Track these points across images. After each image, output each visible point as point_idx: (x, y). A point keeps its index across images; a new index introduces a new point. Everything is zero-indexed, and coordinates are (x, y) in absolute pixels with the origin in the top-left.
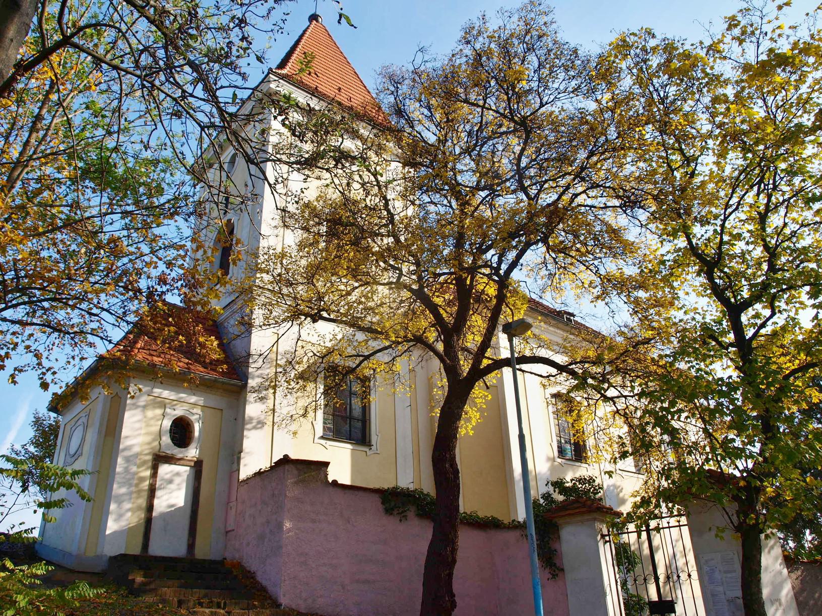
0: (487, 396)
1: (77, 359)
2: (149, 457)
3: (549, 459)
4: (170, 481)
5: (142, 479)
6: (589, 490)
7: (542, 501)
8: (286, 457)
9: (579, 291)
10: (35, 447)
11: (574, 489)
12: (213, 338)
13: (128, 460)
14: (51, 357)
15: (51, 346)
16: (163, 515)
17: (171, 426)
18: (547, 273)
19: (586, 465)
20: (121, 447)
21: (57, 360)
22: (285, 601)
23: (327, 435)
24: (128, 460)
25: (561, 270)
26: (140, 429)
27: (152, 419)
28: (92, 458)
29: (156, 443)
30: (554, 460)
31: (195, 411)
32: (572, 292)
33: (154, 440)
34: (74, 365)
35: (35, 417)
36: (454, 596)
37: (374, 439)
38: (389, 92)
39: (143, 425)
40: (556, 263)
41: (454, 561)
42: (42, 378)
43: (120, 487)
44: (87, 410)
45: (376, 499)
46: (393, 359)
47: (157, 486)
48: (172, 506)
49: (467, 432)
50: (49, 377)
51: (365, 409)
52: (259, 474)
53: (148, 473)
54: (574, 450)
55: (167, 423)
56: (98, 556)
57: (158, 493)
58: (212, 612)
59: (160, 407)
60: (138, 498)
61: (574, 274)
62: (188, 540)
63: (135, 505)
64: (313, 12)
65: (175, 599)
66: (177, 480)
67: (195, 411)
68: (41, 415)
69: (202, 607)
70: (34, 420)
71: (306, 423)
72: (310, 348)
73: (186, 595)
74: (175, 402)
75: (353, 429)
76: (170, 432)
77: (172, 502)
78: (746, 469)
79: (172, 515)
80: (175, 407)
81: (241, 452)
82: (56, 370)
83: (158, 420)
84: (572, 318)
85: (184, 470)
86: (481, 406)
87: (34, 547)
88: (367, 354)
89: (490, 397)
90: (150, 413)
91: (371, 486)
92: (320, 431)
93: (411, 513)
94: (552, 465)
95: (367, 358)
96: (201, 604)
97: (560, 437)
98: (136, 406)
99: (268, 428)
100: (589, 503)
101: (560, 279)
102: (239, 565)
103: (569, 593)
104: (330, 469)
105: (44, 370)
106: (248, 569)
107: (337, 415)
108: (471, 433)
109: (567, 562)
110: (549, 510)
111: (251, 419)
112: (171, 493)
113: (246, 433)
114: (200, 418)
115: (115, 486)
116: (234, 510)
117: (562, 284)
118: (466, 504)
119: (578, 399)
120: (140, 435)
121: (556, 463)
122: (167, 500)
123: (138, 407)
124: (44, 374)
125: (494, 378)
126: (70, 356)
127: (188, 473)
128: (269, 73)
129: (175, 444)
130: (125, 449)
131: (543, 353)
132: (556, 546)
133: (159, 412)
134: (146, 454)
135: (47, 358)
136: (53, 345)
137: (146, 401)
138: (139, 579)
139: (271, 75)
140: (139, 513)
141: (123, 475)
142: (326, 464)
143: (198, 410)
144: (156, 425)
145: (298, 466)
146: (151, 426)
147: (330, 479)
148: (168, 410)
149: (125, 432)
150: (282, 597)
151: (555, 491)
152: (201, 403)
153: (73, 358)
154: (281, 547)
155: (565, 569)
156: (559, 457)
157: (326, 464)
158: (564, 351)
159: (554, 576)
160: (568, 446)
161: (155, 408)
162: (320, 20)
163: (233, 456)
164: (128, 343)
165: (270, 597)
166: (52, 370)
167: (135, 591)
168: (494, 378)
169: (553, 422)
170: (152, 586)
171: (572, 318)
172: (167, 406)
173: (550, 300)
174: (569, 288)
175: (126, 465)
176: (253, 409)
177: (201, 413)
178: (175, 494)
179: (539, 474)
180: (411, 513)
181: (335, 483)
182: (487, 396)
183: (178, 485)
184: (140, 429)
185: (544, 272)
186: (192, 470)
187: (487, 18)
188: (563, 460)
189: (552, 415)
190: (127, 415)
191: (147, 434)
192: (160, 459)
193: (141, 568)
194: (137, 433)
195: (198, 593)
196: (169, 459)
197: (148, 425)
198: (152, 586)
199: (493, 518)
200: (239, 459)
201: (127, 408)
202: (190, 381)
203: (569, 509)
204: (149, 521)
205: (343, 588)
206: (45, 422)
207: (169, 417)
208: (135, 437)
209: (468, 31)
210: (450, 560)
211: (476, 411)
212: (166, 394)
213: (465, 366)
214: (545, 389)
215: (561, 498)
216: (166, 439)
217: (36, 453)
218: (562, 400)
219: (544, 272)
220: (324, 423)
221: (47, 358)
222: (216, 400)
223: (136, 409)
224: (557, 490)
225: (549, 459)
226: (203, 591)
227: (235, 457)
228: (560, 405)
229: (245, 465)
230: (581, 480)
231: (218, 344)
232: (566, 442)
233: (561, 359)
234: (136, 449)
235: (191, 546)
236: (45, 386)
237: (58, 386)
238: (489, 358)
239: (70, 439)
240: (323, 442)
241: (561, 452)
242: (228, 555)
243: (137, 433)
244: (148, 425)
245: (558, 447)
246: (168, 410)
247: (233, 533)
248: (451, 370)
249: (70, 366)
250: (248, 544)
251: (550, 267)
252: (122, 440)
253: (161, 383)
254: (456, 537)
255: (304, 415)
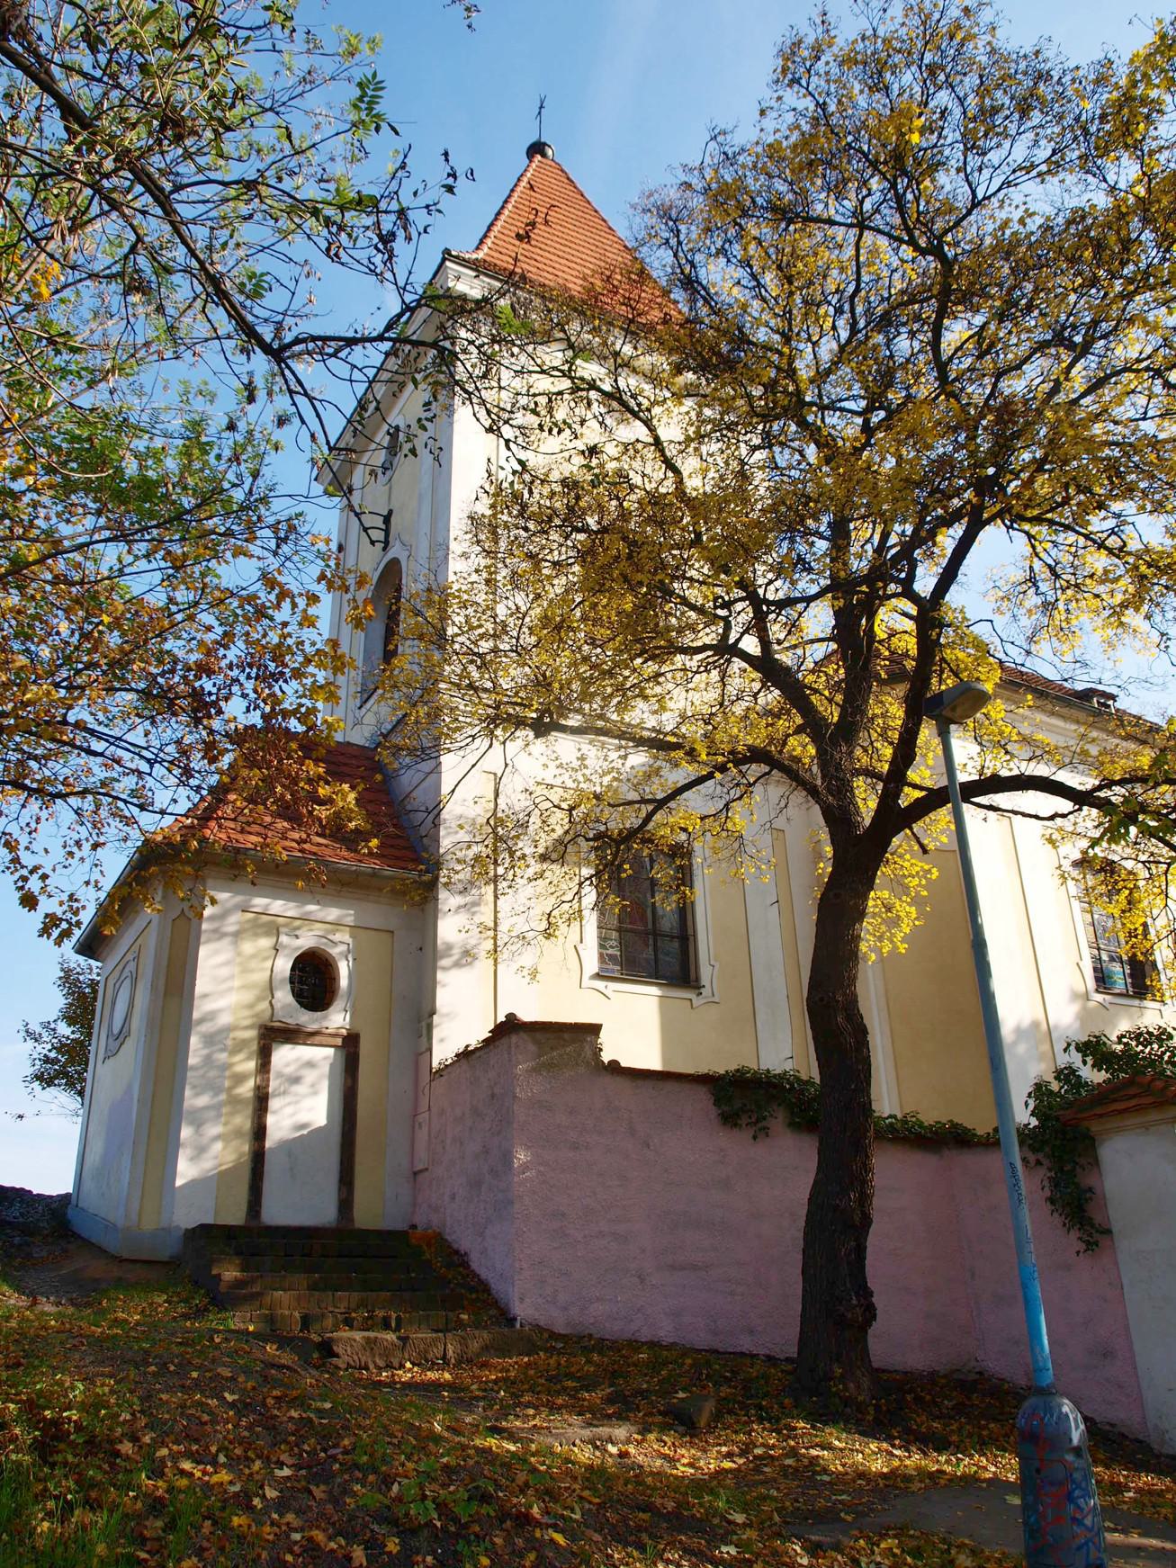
0: (929, 871)
1: (87, 846)
2: (252, 1033)
3: (1075, 996)
4: (296, 1080)
5: (240, 1079)
6: (1161, 1057)
7: (1055, 1086)
8: (511, 1017)
9: (1110, 632)
10: (69, 1025)
11: (1128, 1056)
12: (346, 787)
13: (210, 1040)
14: (34, 847)
15: (33, 825)
16: (288, 1146)
17: (293, 969)
18: (1039, 600)
19: (1157, 1005)
20: (196, 1015)
21: (46, 851)
22: (523, 1310)
23: (607, 970)
24: (210, 1040)
25: (1069, 592)
26: (232, 977)
27: (253, 956)
28: (142, 1043)
29: (264, 1005)
30: (1087, 997)
31: (337, 937)
32: (1097, 637)
33: (259, 999)
34: (82, 859)
35: (62, 970)
36: (871, 1294)
37: (706, 974)
38: (657, 241)
39: (237, 970)
40: (1057, 576)
41: (866, 1221)
42: (22, 888)
43: (197, 1095)
44: (135, 948)
45: (702, 1096)
46: (727, 806)
47: (270, 1090)
48: (303, 1126)
49: (895, 947)
50: (34, 884)
51: (685, 912)
52: (465, 1055)
53: (251, 1065)
54: (1131, 975)
55: (284, 965)
56: (163, 1229)
57: (274, 1104)
58: (368, 1339)
59: (267, 934)
60: (232, 1114)
61: (1097, 596)
62: (340, 1190)
63: (230, 1127)
64: (534, 139)
65: (297, 1314)
66: (310, 1076)
67: (337, 937)
68: (73, 965)
69: (352, 1328)
70: (62, 974)
71: (555, 951)
72: (545, 792)
73: (323, 1305)
74: (298, 923)
75: (661, 956)
76: (291, 982)
77: (303, 1117)
78: (936, 379)
79: (306, 1142)
80: (297, 933)
81: (433, 1012)
82: (48, 871)
83: (266, 959)
84: (1110, 702)
85: (323, 1055)
86: (918, 893)
87: (65, 1214)
88: (660, 796)
89: (935, 874)
90: (248, 947)
91: (691, 1071)
92: (592, 965)
93: (778, 1120)
94: (1084, 1008)
95: (660, 804)
96: (349, 1323)
97: (1099, 949)
98: (219, 934)
99: (484, 965)
100: (1159, 1084)
101: (1068, 611)
102: (438, 1241)
103: (1125, 1281)
104: (604, 1037)
105: (25, 872)
106: (455, 1246)
107: (627, 930)
108: (902, 948)
109: (1117, 1215)
110: (1070, 1104)
111: (449, 947)
112: (297, 1102)
113: (440, 976)
114: (349, 951)
115: (188, 1093)
116: (425, 1129)
117: (1074, 622)
118: (887, 1100)
119: (1129, 864)
120: (230, 989)
121: (1091, 1004)
122: (293, 1114)
123: (225, 935)
124: (25, 879)
125: (942, 832)
126: (72, 843)
127: (331, 1061)
128: (444, 260)
129: (302, 1005)
130: (202, 1021)
131: (1041, 770)
132: (1089, 1180)
133: (266, 943)
134: (246, 1028)
135: (27, 848)
136: (38, 820)
137: (239, 923)
138: (230, 1274)
139: (448, 263)
140: (235, 1143)
141: (201, 1072)
142: (595, 1029)
143: (344, 936)
144: (263, 969)
145: (538, 1036)
146: (252, 971)
147: (606, 1057)
148: (284, 939)
149: (201, 986)
150: (517, 1303)
151: (1085, 1063)
152: (350, 920)
153: (78, 844)
154: (511, 1203)
155: (1115, 1230)
156: (1097, 991)
157: (595, 1029)
158: (1079, 759)
159: (1091, 1245)
160: (1117, 968)
161: (256, 935)
162: (550, 152)
163: (419, 1022)
164: (204, 816)
165: (495, 1303)
166: (40, 872)
167: (221, 1300)
168: (942, 832)
169: (1081, 919)
170: (256, 1289)
171: (1110, 702)
172: (282, 930)
173: (1047, 664)
174: (1088, 627)
175: (205, 1052)
176: (451, 927)
177: (350, 941)
178: (307, 1103)
179: (1056, 1027)
180: (778, 1120)
181: (614, 1065)
182: (929, 871)
183: (313, 1086)
184: (232, 977)
185: (1033, 600)
186: (339, 1054)
187: (830, 18)
188: (1108, 997)
189: (1076, 905)
190: (203, 951)
191: (243, 987)
192: (273, 1034)
193: (238, 1253)
194: (224, 986)
195: (344, 1300)
196: (292, 1035)
197: (245, 971)
198: (256, 1289)
199: (955, 1125)
200: (430, 1027)
201: (203, 939)
202: (307, 877)
203: (1115, 1100)
204: (258, 1157)
205: (642, 1281)
206: (81, 978)
207: (286, 952)
208: (222, 994)
209: (790, 54)
210: (857, 1219)
211: (908, 904)
212: (278, 906)
213: (867, 801)
214: (1055, 848)
215: (1099, 1077)
216: (284, 996)
217: (72, 1036)
218: (1092, 868)
219: (1033, 600)
220: (601, 946)
221: (27, 848)
222: (379, 913)
223: (219, 939)
224: (1089, 1060)
225: (1075, 996)
226: (356, 1296)
227: (424, 1024)
228: (1091, 880)
229: (442, 1040)
230: (1139, 1036)
231: (356, 799)
232: (1112, 959)
233: (1079, 780)
234: (225, 1019)
235: (345, 1204)
236: (29, 901)
237: (55, 901)
238: (915, 786)
239: (114, 1003)
240: (600, 984)
241: (1102, 980)
242: (420, 1220)
243: (224, 986)
244: (245, 971)
245: (1095, 970)
246: (284, 939)
247: (426, 1174)
248: (839, 817)
249: (75, 862)
250: (453, 1197)
251: (1043, 587)
252: (196, 1002)
253: (253, 884)
254: (867, 1168)
255: (548, 934)
